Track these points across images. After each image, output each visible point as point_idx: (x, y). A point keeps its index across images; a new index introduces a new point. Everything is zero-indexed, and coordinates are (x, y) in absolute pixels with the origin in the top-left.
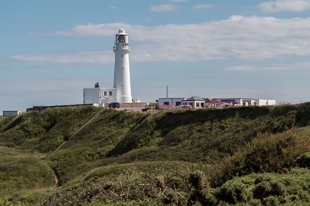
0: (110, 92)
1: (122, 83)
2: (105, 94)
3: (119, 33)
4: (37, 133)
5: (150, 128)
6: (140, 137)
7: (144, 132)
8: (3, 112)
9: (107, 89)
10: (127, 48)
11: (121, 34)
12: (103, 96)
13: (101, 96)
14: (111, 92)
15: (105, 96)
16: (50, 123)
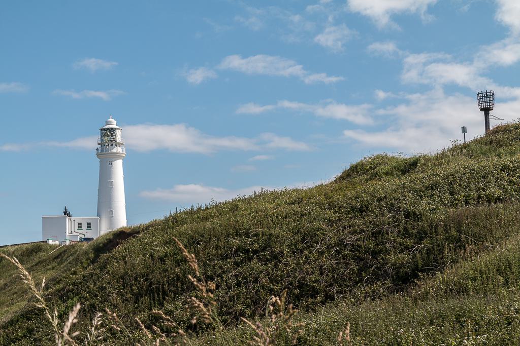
0: (88, 224)
1: (110, 208)
2: (79, 227)
7: (70, 270)
9: (83, 219)
10: (119, 150)
12: (76, 230)
13: (73, 231)
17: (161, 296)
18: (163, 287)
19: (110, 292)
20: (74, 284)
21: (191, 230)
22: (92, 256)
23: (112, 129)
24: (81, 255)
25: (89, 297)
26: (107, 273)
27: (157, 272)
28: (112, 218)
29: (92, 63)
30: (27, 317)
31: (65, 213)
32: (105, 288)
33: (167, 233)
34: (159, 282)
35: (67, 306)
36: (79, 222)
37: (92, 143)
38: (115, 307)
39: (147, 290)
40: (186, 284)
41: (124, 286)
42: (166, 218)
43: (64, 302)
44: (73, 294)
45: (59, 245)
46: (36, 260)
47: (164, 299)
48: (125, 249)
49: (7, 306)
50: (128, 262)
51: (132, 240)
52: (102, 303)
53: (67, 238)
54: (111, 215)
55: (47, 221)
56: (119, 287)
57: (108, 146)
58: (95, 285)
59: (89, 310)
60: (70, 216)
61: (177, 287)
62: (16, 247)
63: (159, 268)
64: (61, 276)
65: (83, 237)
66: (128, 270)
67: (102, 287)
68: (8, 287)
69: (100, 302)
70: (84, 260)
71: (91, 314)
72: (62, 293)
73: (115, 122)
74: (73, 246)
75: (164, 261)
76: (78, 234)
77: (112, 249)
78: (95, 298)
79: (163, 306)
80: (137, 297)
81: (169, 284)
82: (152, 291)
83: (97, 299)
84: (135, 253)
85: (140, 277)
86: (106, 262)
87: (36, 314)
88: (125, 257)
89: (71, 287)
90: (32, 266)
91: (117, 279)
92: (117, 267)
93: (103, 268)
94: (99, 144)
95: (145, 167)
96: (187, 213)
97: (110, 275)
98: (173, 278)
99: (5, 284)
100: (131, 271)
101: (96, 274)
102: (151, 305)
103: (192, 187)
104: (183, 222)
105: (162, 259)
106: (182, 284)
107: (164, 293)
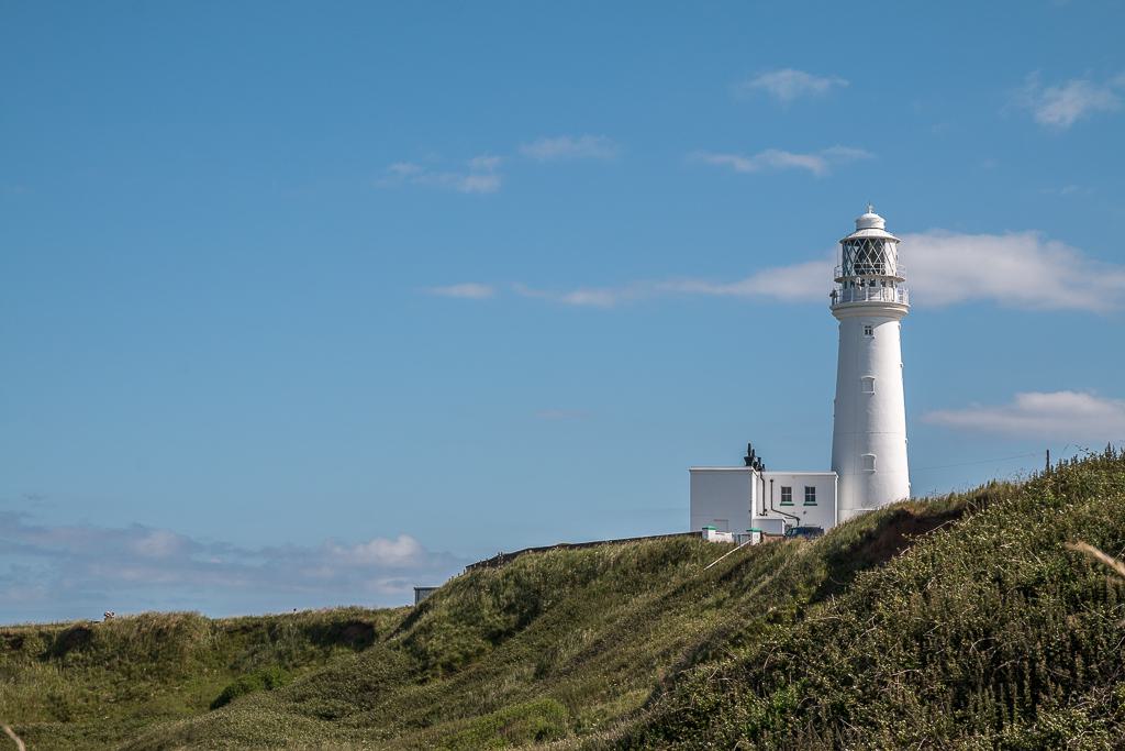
0: (807, 489)
1: (867, 449)
2: (783, 499)
3: (858, 230)
4: (456, 660)
5: (794, 593)
6: (740, 635)
7: (763, 611)
8: (417, 590)
9: (794, 476)
10: (891, 295)
11: (864, 235)
12: (777, 505)
13: (768, 507)
14: (789, 489)
15: (785, 509)
16: (514, 618)
17: (1027, 691)
18: (1033, 668)
19: (885, 674)
20: (787, 648)
21: (1111, 513)
22: (821, 574)
23: (873, 240)
24: (792, 572)
25: (828, 685)
26: (876, 622)
27: (1016, 623)
28: (873, 477)
29: (784, 83)
30: (665, 731)
31: (749, 461)
32: (874, 662)
33: (1040, 519)
34: (1021, 653)
35: (771, 706)
36: (785, 486)
37: (818, 278)
38: (901, 714)
39: (987, 674)
40: (1098, 662)
41: (923, 659)
42: (1036, 479)
43: (762, 696)
44: (786, 674)
45: (735, 545)
46: (676, 581)
47: (1036, 699)
48: (924, 559)
49: (604, 701)
50: (934, 594)
51: (943, 536)
52: (865, 703)
53: (755, 526)
54: (869, 469)
55: (701, 480)
56: (910, 660)
57: (862, 285)
58: (843, 654)
59: (829, 721)
60: (761, 469)
61: (1072, 667)
62: (623, 547)
63: (1022, 615)
64: (742, 625)
65: (794, 523)
66: (934, 615)
67: (863, 659)
68: (605, 650)
69: (858, 699)
70: (801, 586)
71: (834, 732)
72: (756, 670)
73: (881, 223)
74: (769, 549)
75: (1034, 595)
76: (783, 517)
77: (888, 558)
78: (844, 688)
79: (1034, 718)
80: (961, 693)
81: (1050, 659)
82: (1002, 678)
83: (852, 692)
84: (952, 572)
85: (968, 637)
86: (871, 594)
87: (689, 724)
88: (925, 582)
89: (781, 656)
90: (666, 598)
91: (905, 640)
92: (904, 607)
93: (865, 606)
94: (838, 280)
95: (959, 342)
96: (1093, 465)
97: (885, 628)
98: (1061, 644)
99: (598, 643)
100: (943, 619)
101: (847, 624)
102: (999, 714)
103: (1064, 400)
104: (1084, 491)
105: (1028, 591)
106: (1087, 662)
107: (1037, 684)
